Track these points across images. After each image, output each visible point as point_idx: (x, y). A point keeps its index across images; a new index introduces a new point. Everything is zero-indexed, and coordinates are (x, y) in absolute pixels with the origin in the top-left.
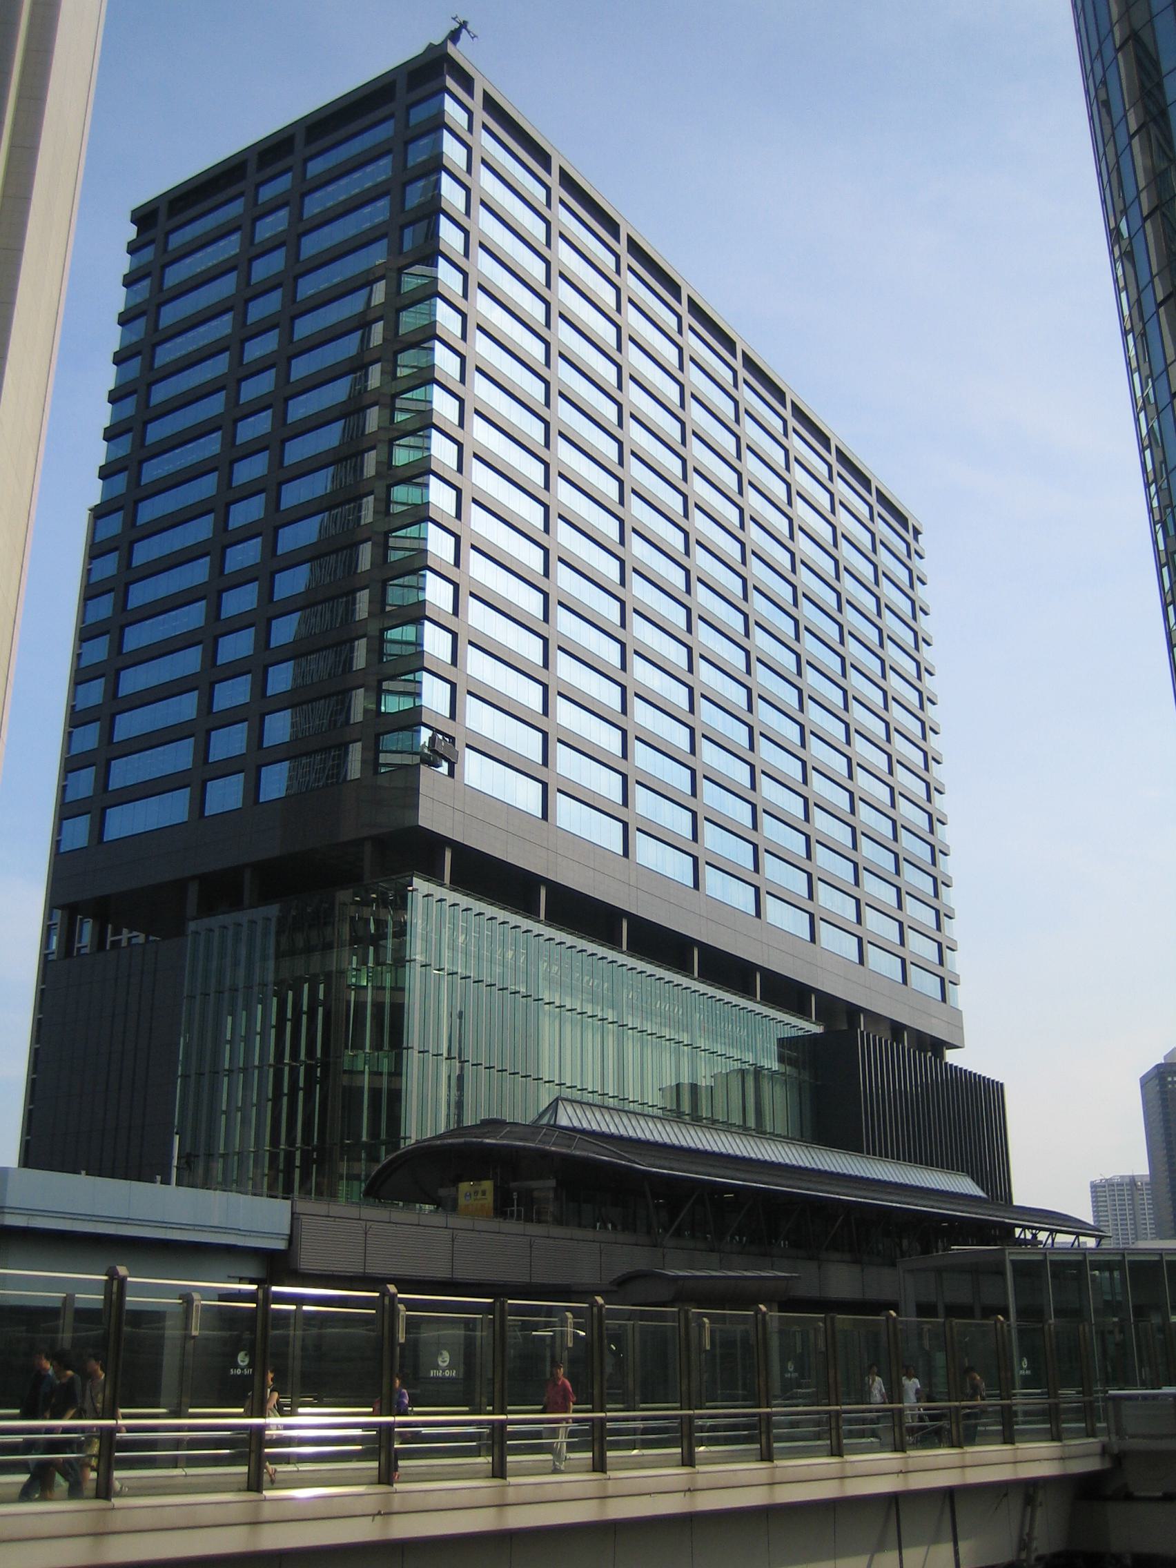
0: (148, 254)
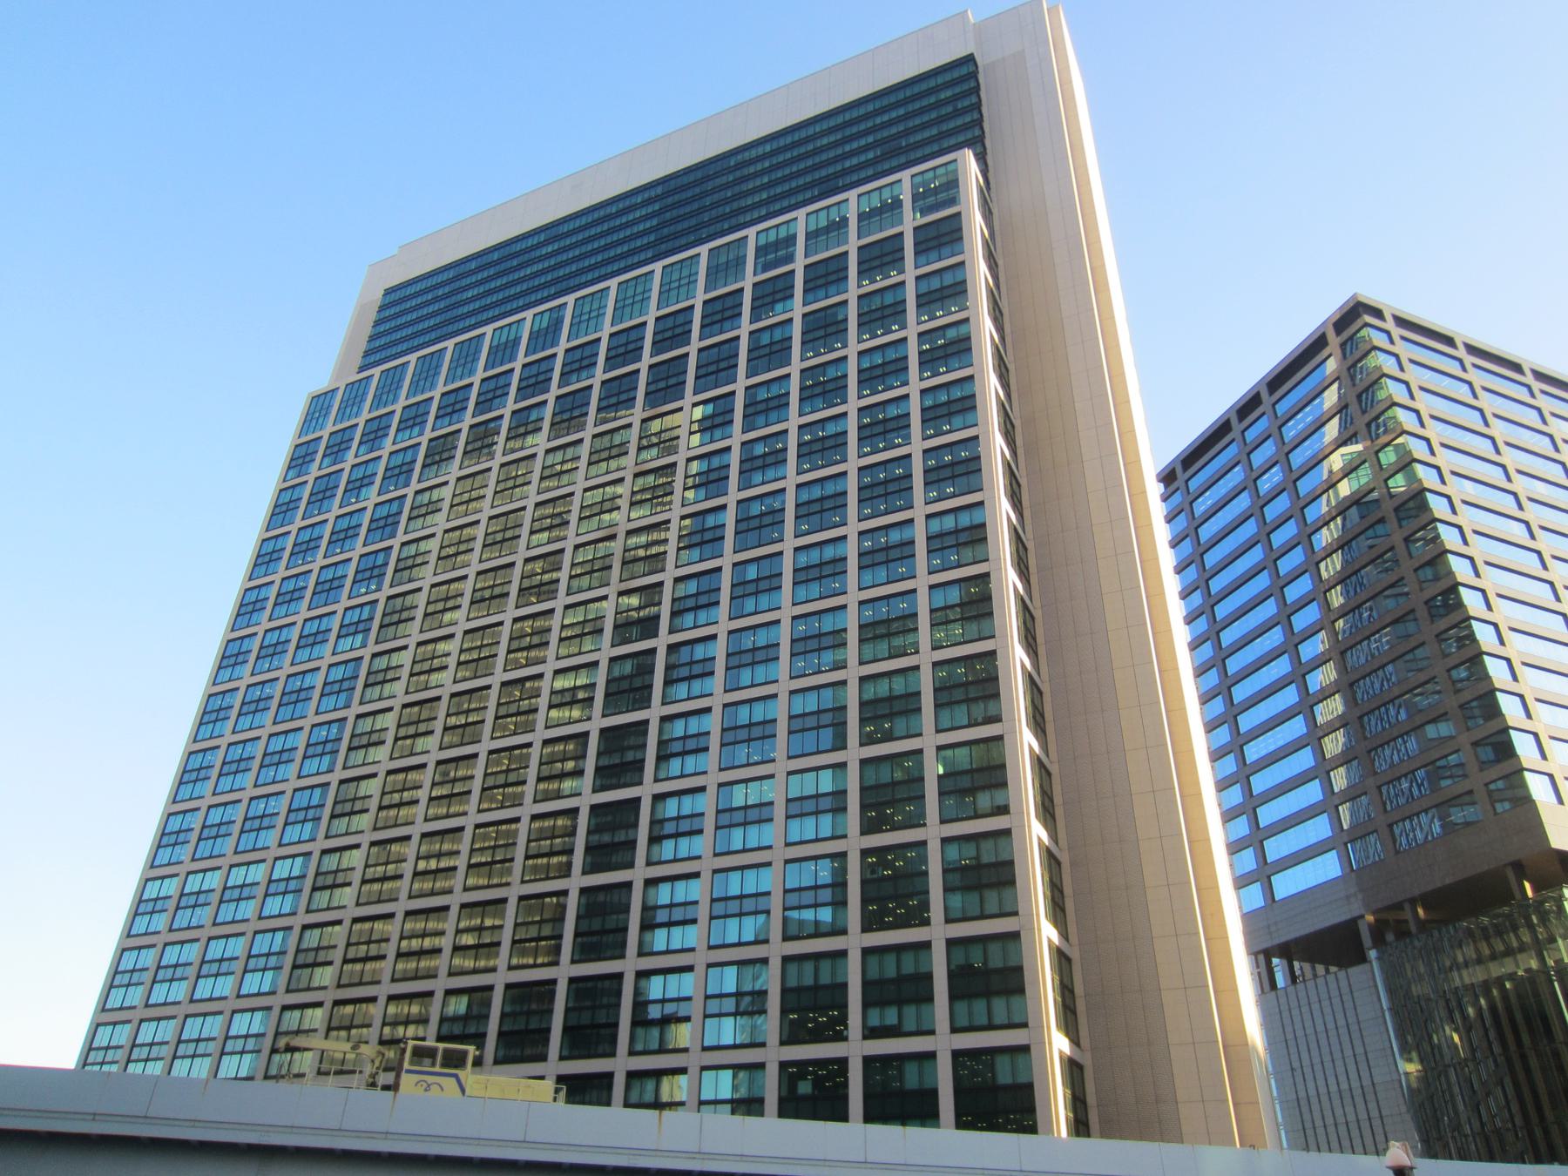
0: (1177, 498)
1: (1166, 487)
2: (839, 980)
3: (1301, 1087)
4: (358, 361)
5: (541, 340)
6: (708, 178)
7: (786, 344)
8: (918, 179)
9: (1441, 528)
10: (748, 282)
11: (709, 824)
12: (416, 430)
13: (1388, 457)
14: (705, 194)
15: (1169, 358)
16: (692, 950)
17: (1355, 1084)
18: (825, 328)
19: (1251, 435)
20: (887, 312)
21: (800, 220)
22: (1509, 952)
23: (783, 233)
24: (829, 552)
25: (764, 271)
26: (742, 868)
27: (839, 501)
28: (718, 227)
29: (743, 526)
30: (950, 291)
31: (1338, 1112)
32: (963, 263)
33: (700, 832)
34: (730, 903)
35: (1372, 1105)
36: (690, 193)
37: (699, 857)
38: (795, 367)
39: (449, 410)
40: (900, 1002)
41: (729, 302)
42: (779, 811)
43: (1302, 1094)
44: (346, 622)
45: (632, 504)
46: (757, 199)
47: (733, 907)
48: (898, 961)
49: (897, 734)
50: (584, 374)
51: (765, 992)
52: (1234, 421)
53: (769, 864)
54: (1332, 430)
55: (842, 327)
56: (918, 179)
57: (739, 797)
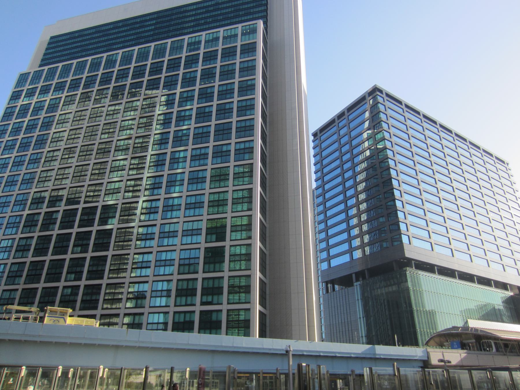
0: (317, 142)
1: (314, 138)
2: (195, 287)
3: (331, 321)
4: (39, 62)
5: (109, 65)
6: (173, 14)
7: (195, 79)
8: (244, 28)
9: (389, 160)
10: (184, 55)
11: (157, 236)
12: (61, 92)
13: (379, 136)
14: (172, 20)
15: (320, 93)
16: (148, 276)
17: (346, 320)
18: (208, 75)
19: (341, 125)
20: (229, 72)
21: (203, 36)
22: (391, 285)
23: (197, 39)
24: (203, 151)
25: (190, 52)
26: (166, 251)
27: (208, 134)
28: (176, 33)
29: (175, 139)
30: (251, 68)
31: (341, 328)
32: (255, 59)
33: (154, 239)
34: (158, 292)
35: (350, 327)
36: (165, 24)
37: (153, 247)
38: (197, 87)
39: (74, 86)
40: (213, 294)
41: (177, 61)
42: (180, 234)
43: (332, 323)
44: (32, 158)
45: (138, 128)
46: (190, 19)
47: (163, 263)
48: (213, 282)
49: (245, 159)
50: (124, 79)
51: (171, 290)
52: (336, 119)
53: (175, 250)
54: (367, 124)
55: (214, 75)
56: (244, 28)
57: (164, 256)
